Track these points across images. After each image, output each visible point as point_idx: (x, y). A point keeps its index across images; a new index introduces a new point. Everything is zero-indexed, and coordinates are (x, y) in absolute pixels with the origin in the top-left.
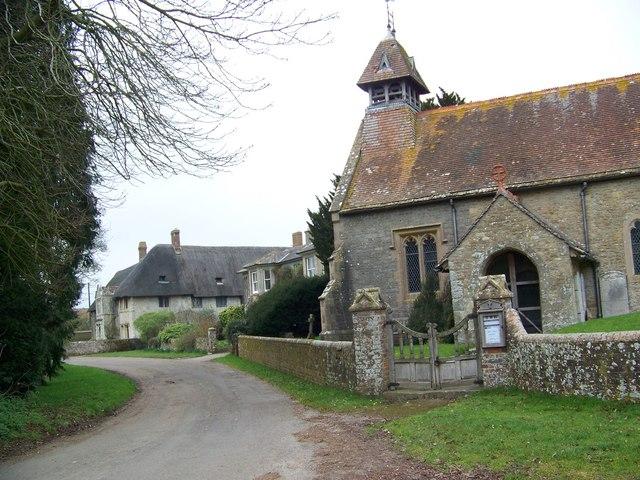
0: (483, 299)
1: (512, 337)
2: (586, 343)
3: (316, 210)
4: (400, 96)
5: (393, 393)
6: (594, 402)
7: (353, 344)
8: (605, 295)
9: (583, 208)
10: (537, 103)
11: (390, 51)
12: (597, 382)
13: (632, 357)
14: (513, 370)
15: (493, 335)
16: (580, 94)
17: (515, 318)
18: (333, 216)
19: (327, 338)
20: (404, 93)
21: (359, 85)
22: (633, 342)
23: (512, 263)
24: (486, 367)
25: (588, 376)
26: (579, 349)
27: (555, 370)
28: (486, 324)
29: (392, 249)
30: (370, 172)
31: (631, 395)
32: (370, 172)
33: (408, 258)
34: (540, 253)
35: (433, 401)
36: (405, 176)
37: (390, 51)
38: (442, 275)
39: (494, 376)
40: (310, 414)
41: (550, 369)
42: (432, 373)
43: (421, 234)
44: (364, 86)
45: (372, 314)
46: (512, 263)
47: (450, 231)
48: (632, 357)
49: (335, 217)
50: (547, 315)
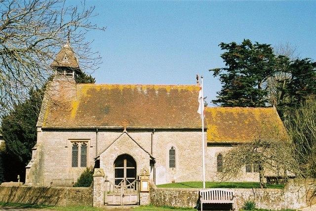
43: (81, 142)
49: (39, 129)
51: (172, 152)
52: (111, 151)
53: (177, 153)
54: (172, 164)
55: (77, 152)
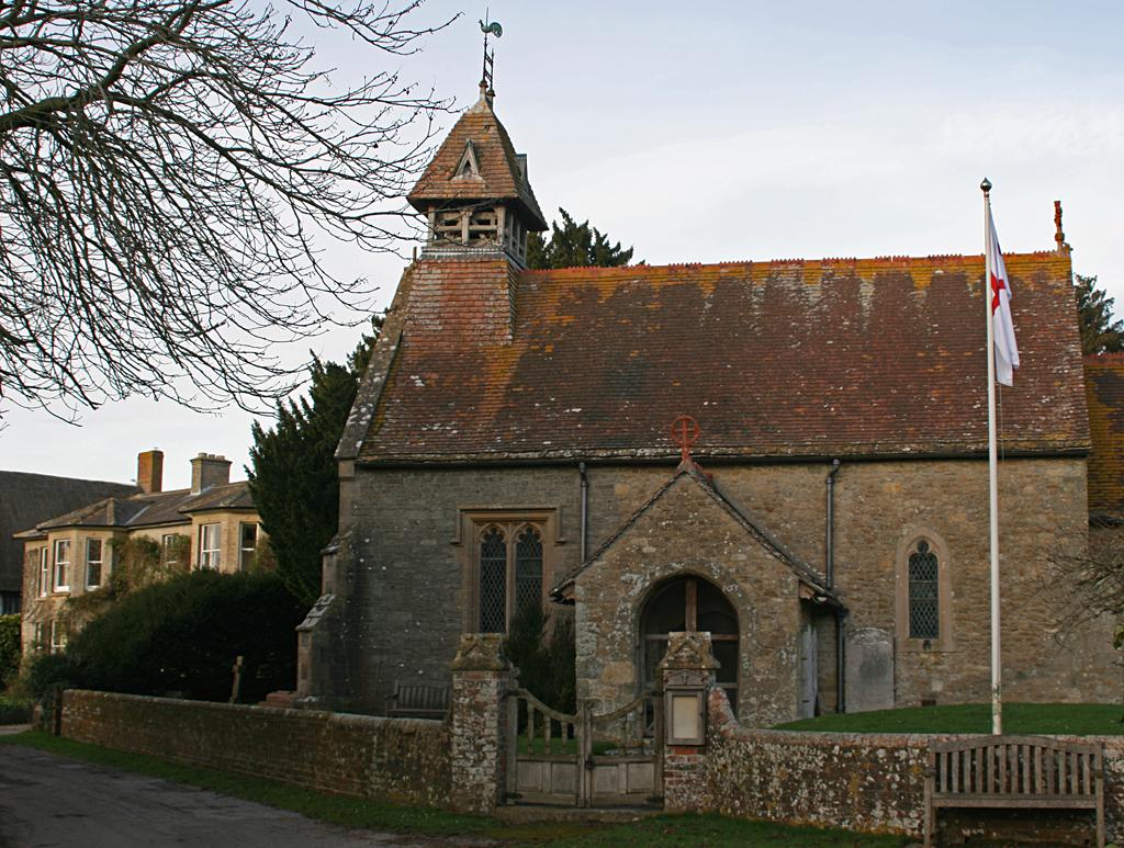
1: (717, 731)
2: (833, 746)
8: (853, 670)
12: (843, 803)
13: (895, 770)
14: (713, 783)
16: (842, 275)
18: (342, 465)
22: (897, 749)
24: (671, 775)
25: (831, 794)
26: (822, 755)
27: (784, 784)
30: (419, 383)
31: (890, 823)
32: (419, 383)
34: (747, 586)
36: (492, 404)
42: (578, 781)
43: (516, 522)
44: (420, 204)
46: (684, 599)
48: (895, 770)
49: (345, 469)
51: (923, 564)
52: (623, 563)
53: (943, 566)
54: (924, 623)
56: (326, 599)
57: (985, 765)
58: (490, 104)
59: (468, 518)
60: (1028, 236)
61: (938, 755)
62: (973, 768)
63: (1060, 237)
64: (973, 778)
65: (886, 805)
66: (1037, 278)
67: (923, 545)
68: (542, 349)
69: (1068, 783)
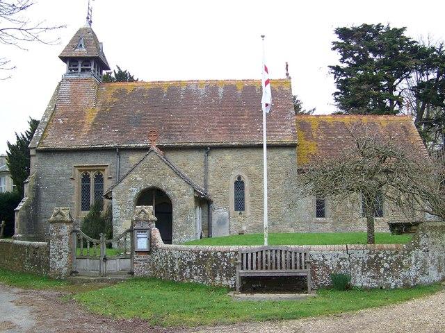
0: (138, 221)
2: (199, 251)
3: (14, 142)
4: (89, 70)
5: (74, 277)
6: (202, 286)
7: (49, 244)
8: (214, 223)
9: (206, 165)
10: (183, 89)
11: (86, 37)
12: (204, 274)
13: (225, 261)
14: (153, 266)
15: (142, 244)
16: (212, 87)
17: (157, 234)
19: (19, 238)
20: (92, 68)
21: (61, 58)
23: (157, 199)
24: (137, 263)
25: (199, 271)
28: (138, 236)
29: (72, 179)
32: (61, 122)
33: (83, 186)
34: (175, 192)
35: (101, 284)
36: (86, 128)
37: (86, 37)
38: (106, 201)
39: (141, 268)
40: (16, 290)
41: (177, 266)
42: (100, 265)
43: (94, 170)
44: (64, 59)
45: (64, 225)
46: (157, 199)
47: (115, 170)
48: (225, 261)
49: (32, 152)
50: (175, 233)
51: (239, 185)
52: (130, 183)
53: (246, 185)
54: (240, 205)
55: (89, 186)
56: (25, 199)
57: (262, 258)
58: (90, 25)
59: (76, 169)
60: (277, 74)
61: (242, 254)
62: (257, 259)
63: (287, 74)
64: (257, 264)
65: (221, 275)
66: (279, 88)
67: (239, 178)
68: (106, 110)
69: (296, 265)
